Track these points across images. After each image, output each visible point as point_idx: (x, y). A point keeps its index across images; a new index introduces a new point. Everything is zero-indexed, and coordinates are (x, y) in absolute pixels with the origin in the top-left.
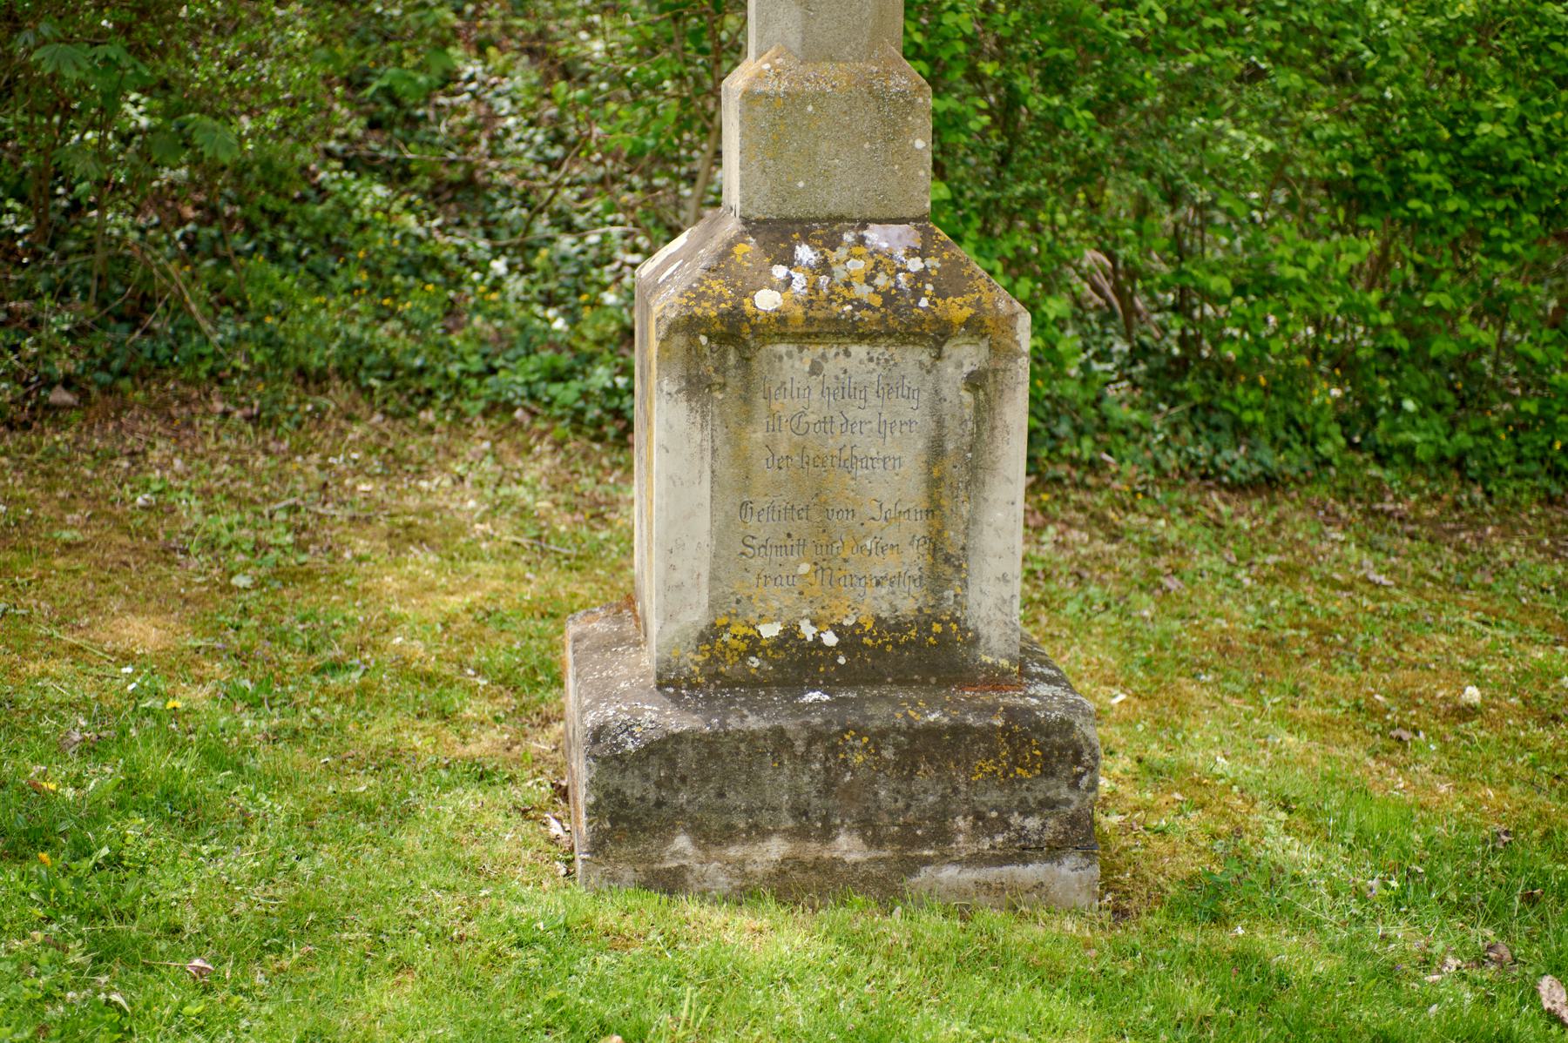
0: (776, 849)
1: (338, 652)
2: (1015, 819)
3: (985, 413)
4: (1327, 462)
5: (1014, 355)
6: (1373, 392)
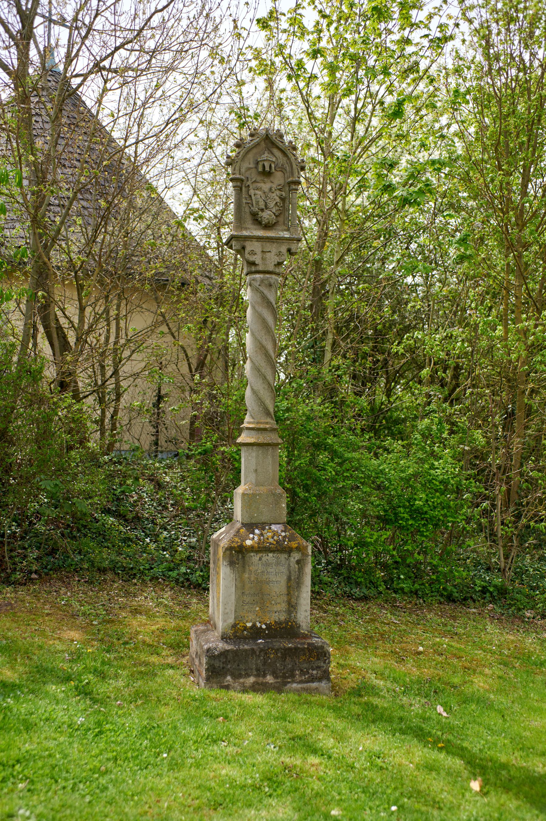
0: (252, 679)
1: (126, 639)
2: (310, 671)
3: (301, 570)
4: (381, 593)
5: (308, 555)
6: (392, 574)
